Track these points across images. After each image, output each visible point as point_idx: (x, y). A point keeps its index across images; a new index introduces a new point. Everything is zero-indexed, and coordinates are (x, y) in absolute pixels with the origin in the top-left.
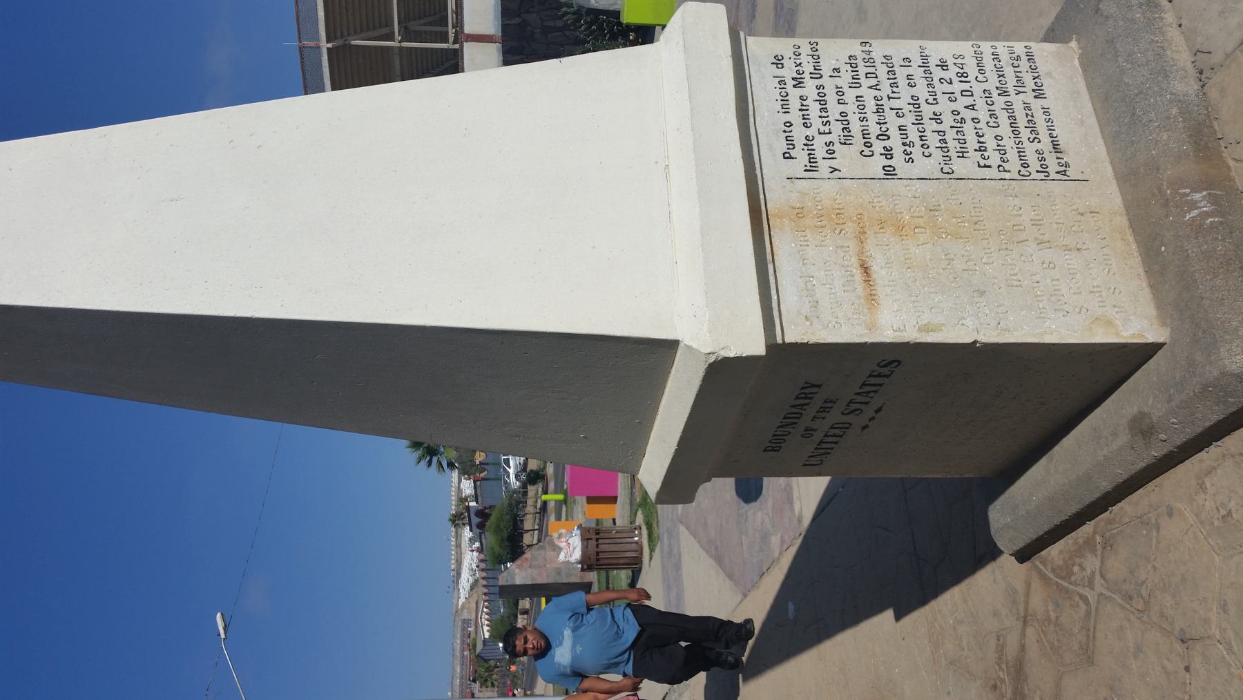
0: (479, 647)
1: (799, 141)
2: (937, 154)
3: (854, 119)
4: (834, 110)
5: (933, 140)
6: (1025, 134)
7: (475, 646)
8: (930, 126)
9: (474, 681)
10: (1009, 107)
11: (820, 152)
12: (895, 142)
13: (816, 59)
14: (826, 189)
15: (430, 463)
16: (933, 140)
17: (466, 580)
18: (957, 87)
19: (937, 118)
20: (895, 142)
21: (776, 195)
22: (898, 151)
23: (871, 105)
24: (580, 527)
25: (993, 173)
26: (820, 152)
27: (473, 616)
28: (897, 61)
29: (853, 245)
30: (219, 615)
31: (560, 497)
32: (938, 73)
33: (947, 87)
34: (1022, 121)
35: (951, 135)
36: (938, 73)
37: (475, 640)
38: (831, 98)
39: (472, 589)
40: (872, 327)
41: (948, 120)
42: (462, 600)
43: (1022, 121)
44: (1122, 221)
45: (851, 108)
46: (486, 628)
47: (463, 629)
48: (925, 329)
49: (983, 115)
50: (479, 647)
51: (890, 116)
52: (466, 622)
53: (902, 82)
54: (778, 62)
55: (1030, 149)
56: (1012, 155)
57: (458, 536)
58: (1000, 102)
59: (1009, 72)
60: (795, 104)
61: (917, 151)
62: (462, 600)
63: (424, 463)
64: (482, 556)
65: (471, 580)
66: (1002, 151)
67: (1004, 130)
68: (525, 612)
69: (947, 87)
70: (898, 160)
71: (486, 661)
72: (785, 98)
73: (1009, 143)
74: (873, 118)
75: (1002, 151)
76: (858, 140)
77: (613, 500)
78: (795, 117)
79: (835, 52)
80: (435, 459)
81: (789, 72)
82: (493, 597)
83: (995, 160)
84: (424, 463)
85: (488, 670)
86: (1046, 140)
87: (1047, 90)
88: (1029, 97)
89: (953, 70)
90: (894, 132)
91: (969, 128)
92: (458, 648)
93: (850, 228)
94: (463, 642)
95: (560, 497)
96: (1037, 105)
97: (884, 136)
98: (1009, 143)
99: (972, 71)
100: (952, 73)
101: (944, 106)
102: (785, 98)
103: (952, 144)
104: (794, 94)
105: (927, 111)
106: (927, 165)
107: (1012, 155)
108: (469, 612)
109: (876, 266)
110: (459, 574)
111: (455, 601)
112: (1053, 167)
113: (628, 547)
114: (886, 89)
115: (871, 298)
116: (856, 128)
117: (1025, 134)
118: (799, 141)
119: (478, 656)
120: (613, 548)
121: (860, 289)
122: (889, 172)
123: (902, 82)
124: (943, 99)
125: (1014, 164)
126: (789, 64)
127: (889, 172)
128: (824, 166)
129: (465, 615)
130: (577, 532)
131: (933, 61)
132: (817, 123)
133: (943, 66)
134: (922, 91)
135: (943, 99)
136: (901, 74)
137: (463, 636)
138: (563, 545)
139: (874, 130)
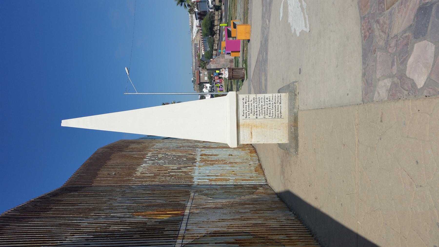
0: (201, 57)
1: (245, 113)
2: (264, 114)
3: (253, 109)
4: (250, 107)
5: (263, 112)
6: (277, 110)
7: (199, 56)
8: (263, 110)
9: (200, 67)
10: (275, 106)
11: (248, 115)
12: (258, 113)
13: (249, 98)
14: (248, 121)
15: (182, 5)
16: (263, 112)
17: (195, 29)
18: (269, 102)
19: (264, 108)
20: (258, 113)
21: (241, 122)
22: (258, 115)
23: (255, 107)
24: (229, 68)
25: (271, 117)
26: (248, 115)
27: (198, 42)
28: (260, 98)
29: (250, 129)
30: (126, 68)
31: (226, 25)
32: (266, 100)
33: (267, 103)
34: (277, 108)
35: (266, 111)
36: (266, 100)
37: (199, 54)
38: (250, 105)
39: (197, 33)
40: (251, 142)
41: (266, 109)
42: (194, 37)
43: (277, 108)
44: (287, 125)
45: (253, 107)
46: (203, 51)
47: (195, 47)
48: (257, 142)
49: (271, 108)
50: (201, 57)
51: (258, 108)
52: (196, 45)
53: (261, 102)
54: (243, 99)
55: (277, 113)
56: (274, 114)
57: (192, 17)
58: (274, 105)
59: (277, 99)
60: (245, 106)
61: (261, 114)
62: (194, 37)
63: (179, 5)
64: (200, 28)
65: (197, 30)
66: (273, 114)
67: (274, 110)
68: (216, 50)
69: (267, 103)
70: (258, 116)
71: (203, 61)
72: (244, 106)
73: (274, 112)
74: (256, 109)
75: (273, 114)
76: (253, 113)
77: (239, 52)
78: (245, 109)
79: (252, 96)
80: (183, 3)
81: (244, 101)
82: (205, 42)
83: (271, 115)
84: (179, 5)
85: (204, 64)
86: (279, 111)
87: (282, 103)
88: (279, 104)
89: (269, 99)
90: (258, 111)
91: (269, 110)
92: (194, 53)
93: (250, 127)
94: (195, 54)
95: (226, 25)
96: (279, 105)
97: (257, 112)
98: (274, 112)
99: (271, 100)
100: (268, 100)
101: (266, 106)
102: (244, 106)
103: (266, 113)
104: (245, 105)
105: (263, 107)
106: (262, 117)
107: (274, 114)
108: (197, 41)
109: (253, 134)
110: (192, 27)
111: (192, 37)
112: (280, 116)
113: (241, 74)
114: (258, 103)
115: (252, 137)
116: (253, 111)
117: (277, 110)
118: (245, 113)
119: (201, 60)
120: (237, 74)
121: (250, 136)
122: (257, 118)
123: (261, 102)
124: (266, 105)
125: (274, 116)
126: (245, 99)
127: (257, 118)
128: (248, 117)
129: (195, 42)
130: (227, 70)
131: (266, 98)
132: (248, 110)
133: (267, 99)
134: (263, 104)
135: (266, 105)
136: (261, 100)
137: (195, 49)
138: (223, 73)
139: (255, 111)
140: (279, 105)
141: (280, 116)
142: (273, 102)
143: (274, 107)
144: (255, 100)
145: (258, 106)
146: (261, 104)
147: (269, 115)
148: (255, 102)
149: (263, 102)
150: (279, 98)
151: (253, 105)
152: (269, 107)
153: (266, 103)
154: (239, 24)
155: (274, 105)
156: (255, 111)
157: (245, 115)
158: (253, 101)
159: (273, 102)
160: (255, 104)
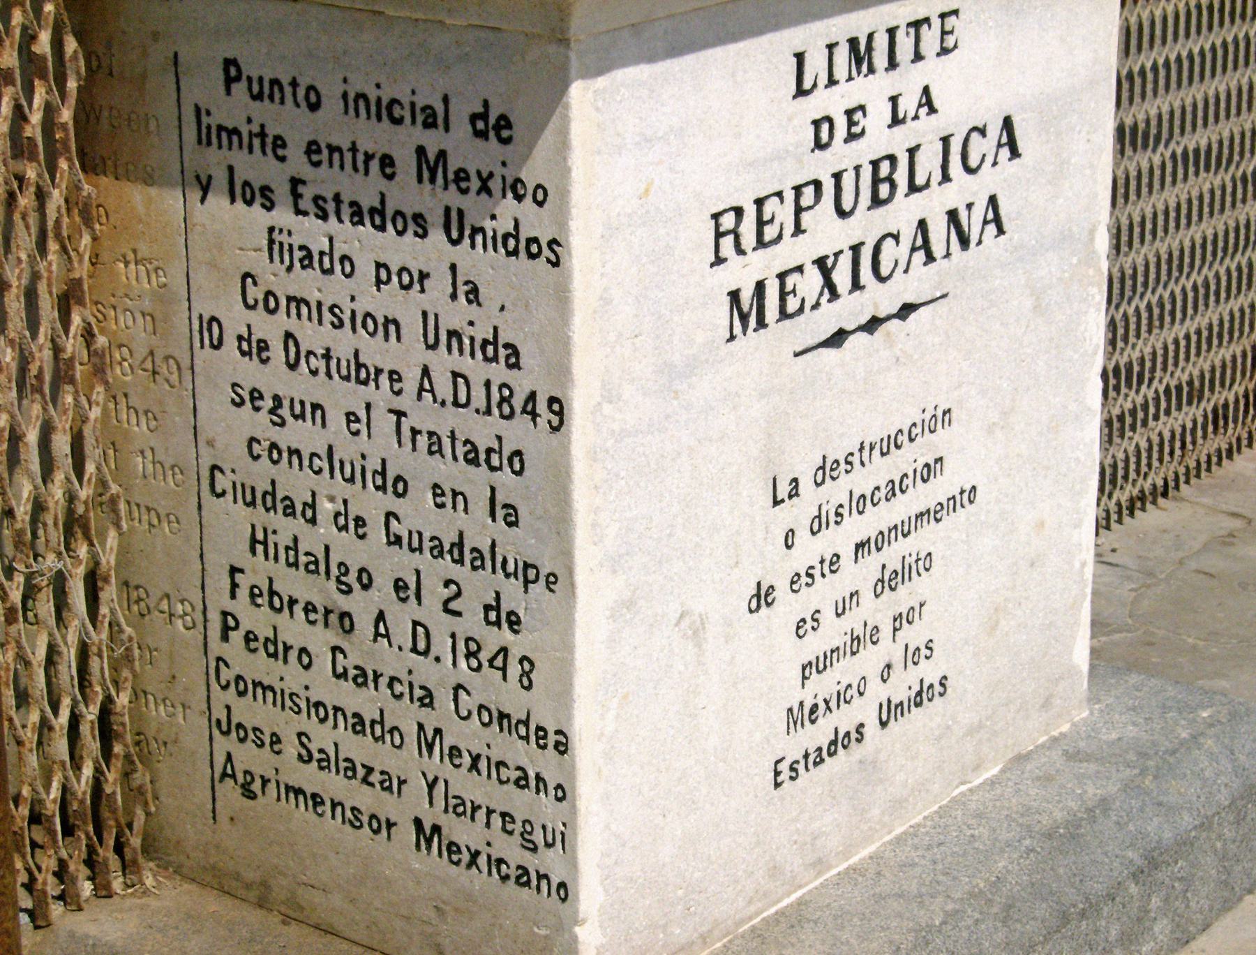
22: (250, 373)
23: (376, 352)
25: (219, 599)
36: (479, 587)
41: (347, 549)
55: (287, 724)
58: (406, 716)
60: (374, 136)
66: (276, 649)
72: (388, 111)
76: (273, 276)
78: (332, 125)
102: (388, 111)
104: (403, 142)
114: (423, 416)
116: (308, 283)
124: (403, 563)
134: (419, 513)
140: (864, 711)
141: (249, 757)
142: (442, 714)
143: (366, 702)
144: (476, 369)
145: (381, 395)
146: (423, 469)
147: (258, 570)
148: (443, 362)
149: (445, 525)
150: (514, 853)
151: (388, 302)
152: (361, 606)
153: (436, 570)
154: (38, 712)
155: (406, 716)
156: (313, 336)
157: (235, 109)
158: (455, 315)
159: (442, 714)
160: (407, 355)
